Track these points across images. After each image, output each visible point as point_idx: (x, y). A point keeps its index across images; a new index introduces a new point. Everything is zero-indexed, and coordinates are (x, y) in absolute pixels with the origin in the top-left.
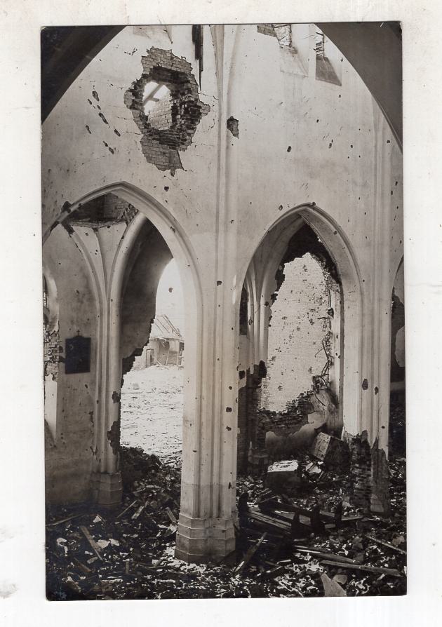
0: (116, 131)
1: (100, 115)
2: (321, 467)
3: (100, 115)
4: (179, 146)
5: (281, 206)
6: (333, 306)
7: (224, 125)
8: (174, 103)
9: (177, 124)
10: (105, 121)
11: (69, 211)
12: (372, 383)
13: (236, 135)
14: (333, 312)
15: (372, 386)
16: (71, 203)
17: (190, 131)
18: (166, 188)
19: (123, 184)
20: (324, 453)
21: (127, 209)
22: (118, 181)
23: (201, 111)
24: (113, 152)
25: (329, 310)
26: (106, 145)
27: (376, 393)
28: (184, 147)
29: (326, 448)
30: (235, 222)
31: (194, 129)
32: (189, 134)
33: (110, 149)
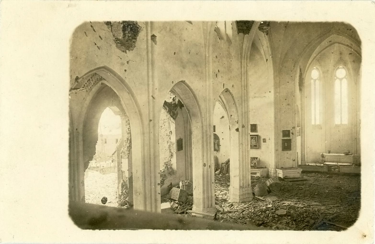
0: (100, 37)
1: (92, 26)
2: (177, 203)
3: (92, 26)
4: (130, 48)
5: (173, 82)
6: (171, 130)
7: (149, 38)
8: (124, 25)
9: (126, 36)
10: (94, 30)
11: (78, 82)
12: (208, 164)
13: (156, 44)
14: (171, 133)
15: (208, 165)
16: (79, 77)
17: (134, 40)
18: (125, 70)
19: (104, 67)
20: (178, 197)
21: (86, 83)
22: (102, 65)
23: (139, 30)
24: (99, 49)
25: (170, 132)
26: (96, 44)
27: (209, 168)
28: (132, 48)
29: (179, 194)
30: (157, 89)
31: (136, 39)
32: (134, 42)
33: (97, 46)
